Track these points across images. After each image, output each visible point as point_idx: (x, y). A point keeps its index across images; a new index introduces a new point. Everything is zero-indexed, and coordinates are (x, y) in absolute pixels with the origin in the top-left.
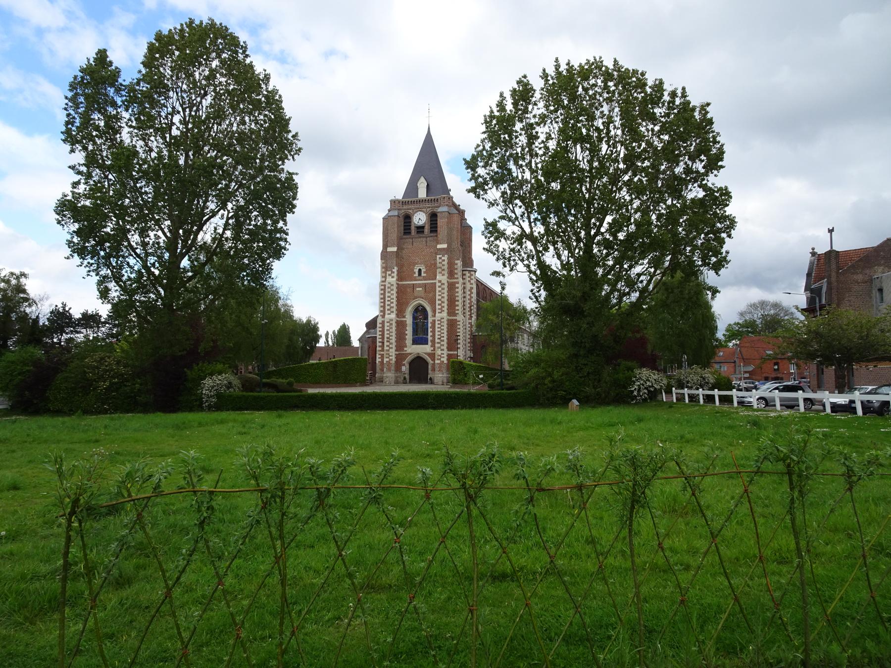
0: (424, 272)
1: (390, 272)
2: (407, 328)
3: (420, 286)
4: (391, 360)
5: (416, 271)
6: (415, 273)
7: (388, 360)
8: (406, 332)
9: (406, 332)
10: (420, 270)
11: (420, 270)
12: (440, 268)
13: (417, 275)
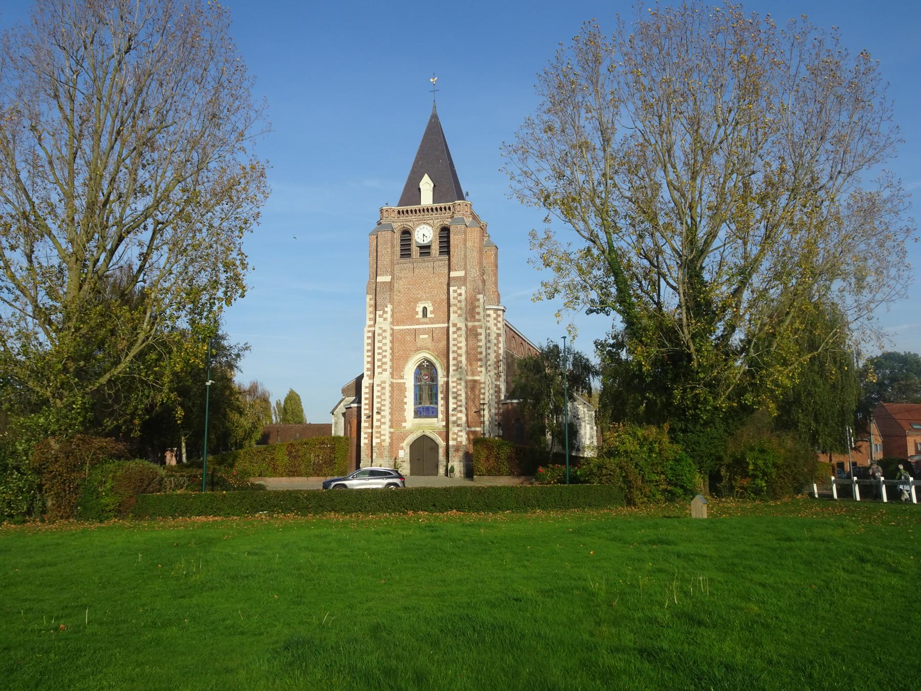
0: (432, 312)
1: (381, 313)
2: (407, 394)
3: (424, 331)
4: (384, 440)
5: (420, 310)
6: (417, 313)
7: (378, 440)
8: (405, 400)
9: (405, 400)
10: (425, 309)
11: (425, 309)
12: (455, 305)
13: (420, 315)
